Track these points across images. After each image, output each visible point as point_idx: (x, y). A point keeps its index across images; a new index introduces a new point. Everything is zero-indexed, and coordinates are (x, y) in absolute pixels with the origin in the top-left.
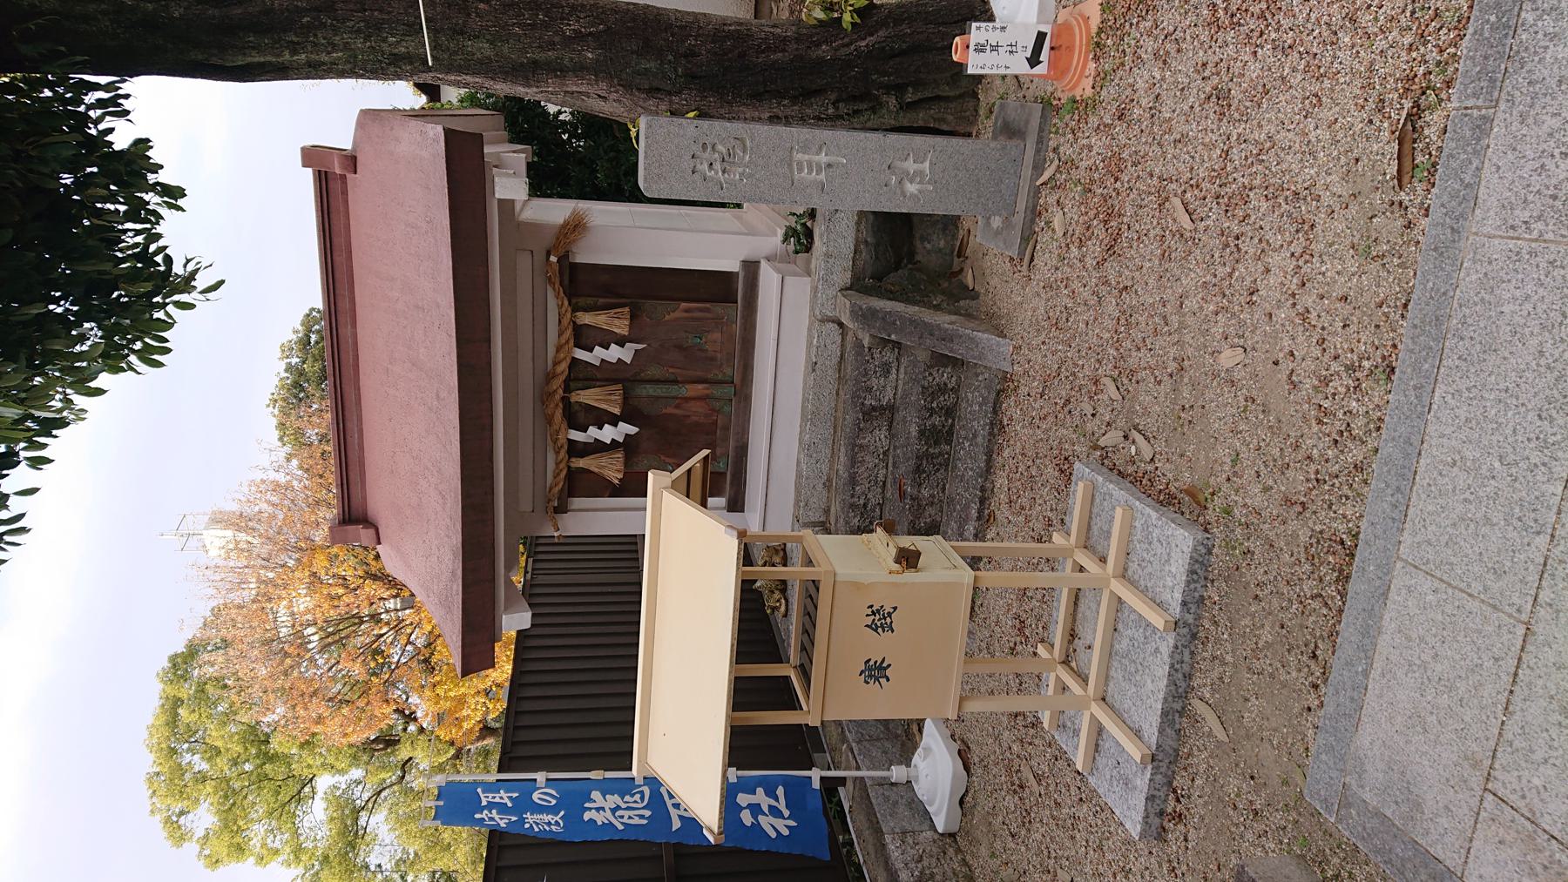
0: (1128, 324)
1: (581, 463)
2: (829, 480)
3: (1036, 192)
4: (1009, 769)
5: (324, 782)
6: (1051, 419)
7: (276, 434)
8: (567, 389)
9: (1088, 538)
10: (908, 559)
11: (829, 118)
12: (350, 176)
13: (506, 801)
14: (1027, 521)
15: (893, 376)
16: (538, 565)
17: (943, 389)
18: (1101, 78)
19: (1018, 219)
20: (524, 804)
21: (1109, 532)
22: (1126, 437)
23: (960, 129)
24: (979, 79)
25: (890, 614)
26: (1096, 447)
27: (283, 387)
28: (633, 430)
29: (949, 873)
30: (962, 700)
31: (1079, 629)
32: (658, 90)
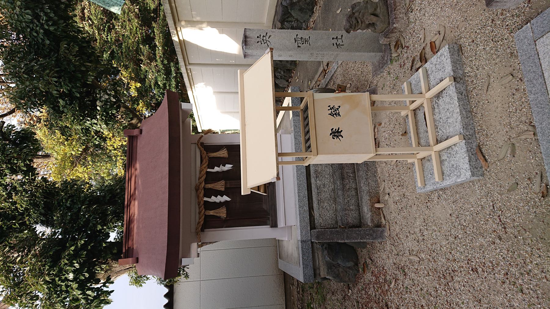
1: (212, 213)
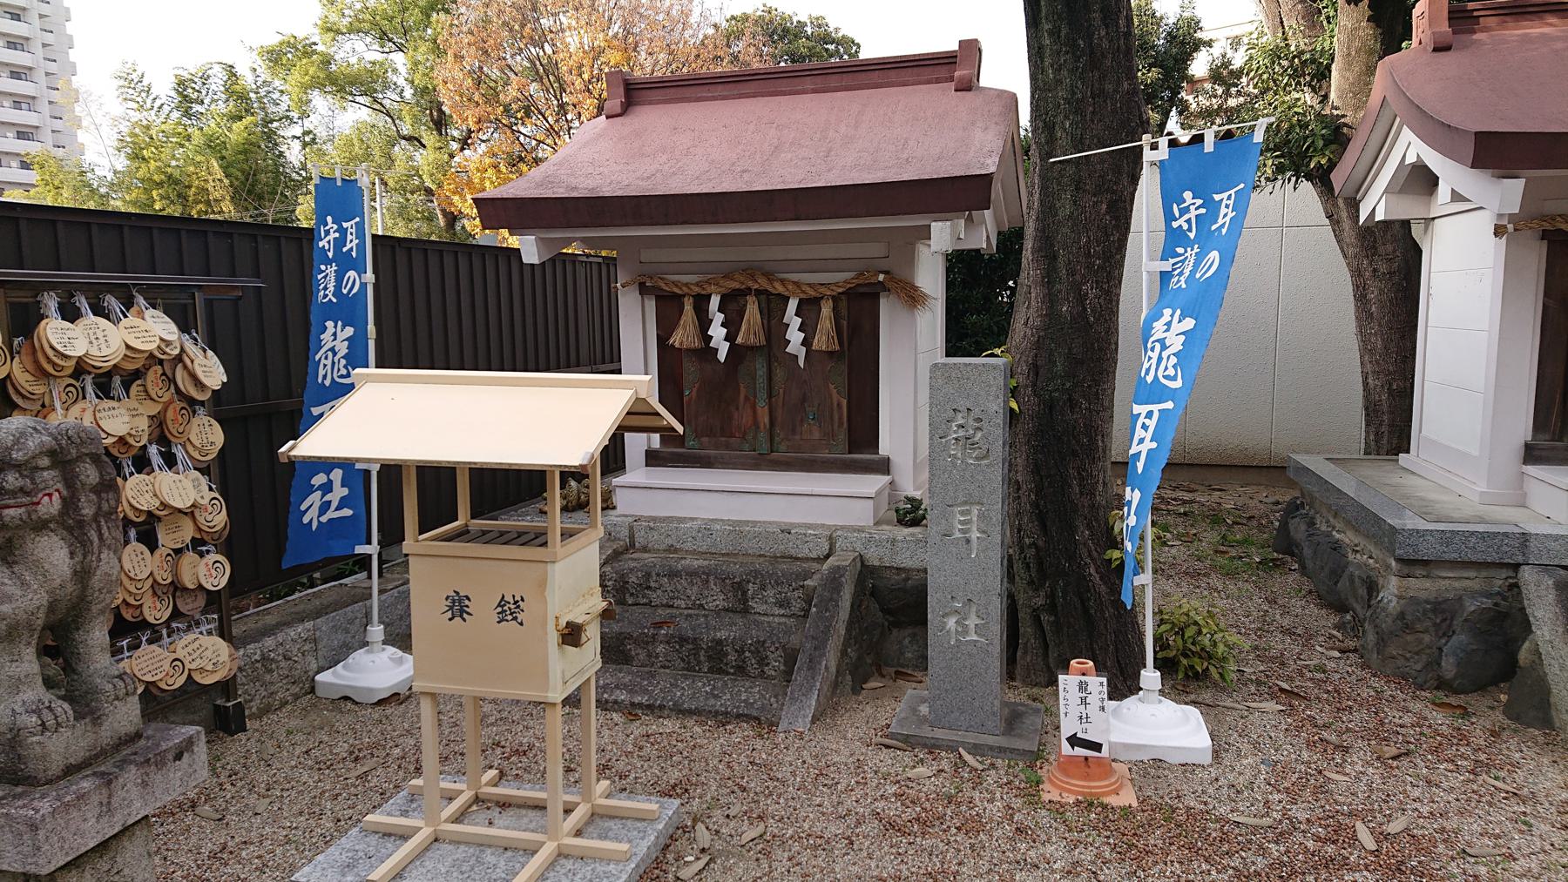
0: (816, 847)
1: (688, 307)
2: (676, 551)
3: (952, 748)
4: (376, 745)
5: (399, 59)
6: (728, 773)
7: (738, 13)
8: (758, 293)
9: (602, 817)
10: (572, 635)
11: (1021, 539)
12: (952, 85)
13: (349, 246)
14: (627, 754)
15: (777, 611)
16: (595, 267)
17: (763, 662)
18: (1058, 809)
19: (927, 732)
20: (346, 262)
21: (606, 838)
22: (703, 850)
23: (1018, 670)
24: (1055, 682)
25: (515, 619)
26: (695, 821)
27: (783, 19)
28: (722, 356)
29: (273, 688)
30: (433, 696)
31: (511, 812)
32: (1037, 374)
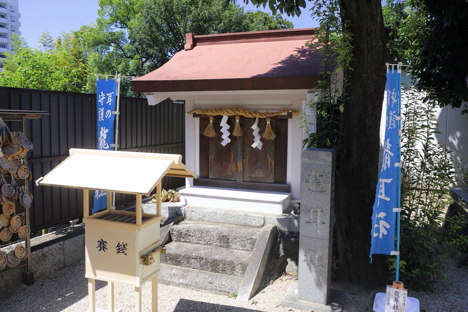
13: (108, 102)
25: (124, 252)
